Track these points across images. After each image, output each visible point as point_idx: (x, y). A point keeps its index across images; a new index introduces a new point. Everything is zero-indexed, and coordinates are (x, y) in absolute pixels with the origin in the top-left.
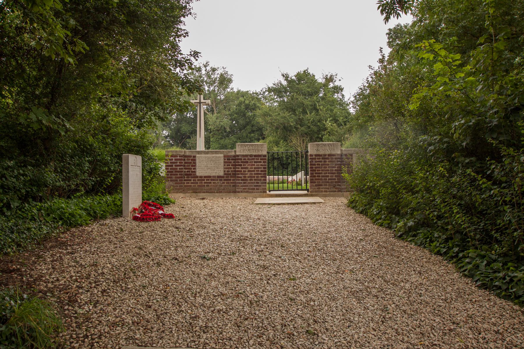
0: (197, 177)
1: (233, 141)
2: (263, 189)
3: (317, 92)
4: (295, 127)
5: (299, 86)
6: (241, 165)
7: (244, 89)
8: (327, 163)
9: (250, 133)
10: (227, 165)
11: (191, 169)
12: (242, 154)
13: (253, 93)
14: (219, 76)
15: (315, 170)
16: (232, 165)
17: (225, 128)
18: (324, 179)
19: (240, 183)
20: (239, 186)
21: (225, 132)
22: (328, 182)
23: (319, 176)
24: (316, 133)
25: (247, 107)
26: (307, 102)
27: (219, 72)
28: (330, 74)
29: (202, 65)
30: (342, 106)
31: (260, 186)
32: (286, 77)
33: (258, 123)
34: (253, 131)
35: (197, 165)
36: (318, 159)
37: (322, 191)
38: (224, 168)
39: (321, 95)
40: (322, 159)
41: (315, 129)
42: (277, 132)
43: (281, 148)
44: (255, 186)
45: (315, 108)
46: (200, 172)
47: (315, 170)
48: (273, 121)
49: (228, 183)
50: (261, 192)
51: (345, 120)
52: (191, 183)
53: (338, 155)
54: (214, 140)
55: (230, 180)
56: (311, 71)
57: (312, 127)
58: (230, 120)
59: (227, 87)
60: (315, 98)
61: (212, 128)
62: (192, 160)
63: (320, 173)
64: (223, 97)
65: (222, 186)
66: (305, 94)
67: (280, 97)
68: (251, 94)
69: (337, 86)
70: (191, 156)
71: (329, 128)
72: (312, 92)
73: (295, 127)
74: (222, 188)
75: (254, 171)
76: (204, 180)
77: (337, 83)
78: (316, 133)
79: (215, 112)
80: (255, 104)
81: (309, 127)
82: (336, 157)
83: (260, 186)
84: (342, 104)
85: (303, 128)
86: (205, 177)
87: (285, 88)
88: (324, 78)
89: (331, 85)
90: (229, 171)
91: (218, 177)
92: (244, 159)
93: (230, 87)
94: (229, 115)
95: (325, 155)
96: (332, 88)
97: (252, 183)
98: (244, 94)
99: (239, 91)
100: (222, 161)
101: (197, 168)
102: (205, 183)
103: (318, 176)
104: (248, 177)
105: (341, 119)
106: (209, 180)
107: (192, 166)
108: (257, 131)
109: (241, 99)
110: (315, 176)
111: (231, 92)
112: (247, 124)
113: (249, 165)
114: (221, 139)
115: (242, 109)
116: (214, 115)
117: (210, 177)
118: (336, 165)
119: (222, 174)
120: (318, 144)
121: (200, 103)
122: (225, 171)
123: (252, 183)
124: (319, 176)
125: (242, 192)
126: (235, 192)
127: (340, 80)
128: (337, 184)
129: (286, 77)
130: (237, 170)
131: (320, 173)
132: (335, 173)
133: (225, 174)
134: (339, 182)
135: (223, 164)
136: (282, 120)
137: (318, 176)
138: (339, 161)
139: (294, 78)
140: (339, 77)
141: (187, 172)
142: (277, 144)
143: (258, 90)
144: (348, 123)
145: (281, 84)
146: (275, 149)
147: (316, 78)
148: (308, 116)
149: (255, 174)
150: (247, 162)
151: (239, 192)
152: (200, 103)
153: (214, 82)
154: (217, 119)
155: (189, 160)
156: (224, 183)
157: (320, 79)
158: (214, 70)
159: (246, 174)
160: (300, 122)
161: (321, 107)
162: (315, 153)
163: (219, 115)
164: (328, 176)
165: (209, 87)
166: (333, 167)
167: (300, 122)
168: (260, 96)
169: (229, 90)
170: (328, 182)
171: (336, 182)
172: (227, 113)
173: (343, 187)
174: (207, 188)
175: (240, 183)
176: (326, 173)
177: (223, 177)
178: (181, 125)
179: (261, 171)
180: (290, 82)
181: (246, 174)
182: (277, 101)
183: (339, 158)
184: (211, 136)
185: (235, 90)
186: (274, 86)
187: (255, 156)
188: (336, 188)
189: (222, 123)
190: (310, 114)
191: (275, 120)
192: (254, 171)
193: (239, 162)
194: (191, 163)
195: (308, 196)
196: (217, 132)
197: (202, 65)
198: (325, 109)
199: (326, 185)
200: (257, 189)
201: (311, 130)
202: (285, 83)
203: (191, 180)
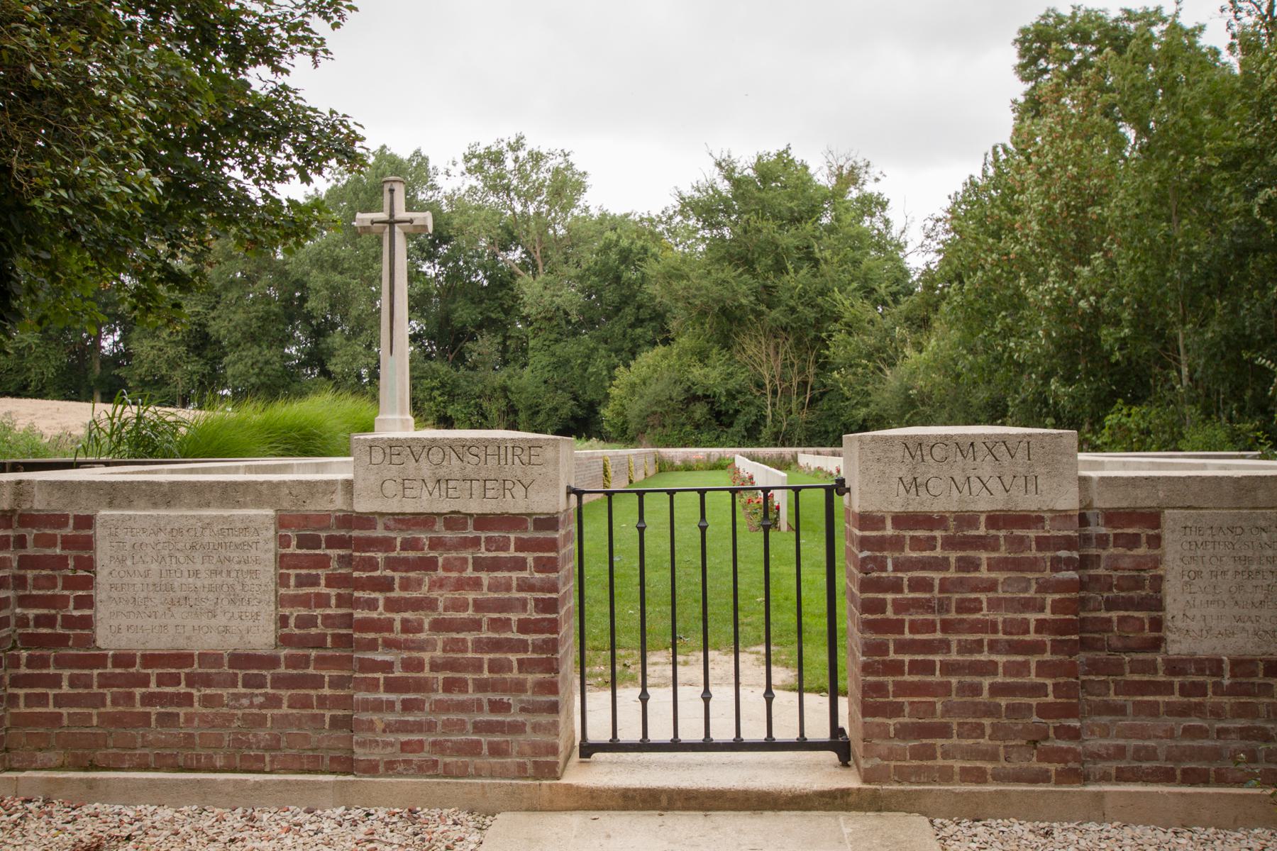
0: (99, 660)
1: (588, 348)
2: (537, 749)
3: (813, 211)
4: (753, 311)
5: (763, 195)
6: (385, 585)
7: (616, 210)
8: (984, 573)
9: (632, 326)
10: (301, 582)
11: (61, 602)
12: (394, 506)
13: (642, 220)
14: (549, 176)
15: (897, 626)
16: (330, 582)
17: (566, 313)
18: (962, 689)
19: (378, 706)
20: (370, 726)
21: (569, 322)
22: (992, 711)
23: (928, 668)
25: (625, 256)
26: (788, 239)
27: (553, 163)
28: (851, 162)
30: (885, 249)
31: (517, 728)
32: (726, 168)
33: (652, 298)
34: (639, 322)
35: (102, 576)
36: (917, 543)
37: (946, 775)
38: (281, 601)
39: (825, 221)
40: (949, 543)
41: (811, 314)
42: (702, 324)
43: (714, 368)
44: (479, 728)
45: (808, 256)
46: (121, 624)
47: (897, 626)
48: (693, 291)
49: (305, 703)
50: (521, 772)
51: (894, 288)
52: (60, 701)
53: (1063, 516)
55: (317, 682)
56: (797, 155)
57: (800, 308)
58: (582, 291)
59: (571, 204)
60: (809, 226)
61: (534, 311)
62: (67, 543)
63: (929, 647)
64: (561, 232)
65: (259, 721)
66: (780, 234)
67: (712, 226)
68: (635, 223)
69: (871, 195)
70: (60, 520)
71: (847, 314)
73: (753, 311)
75: (475, 625)
76: (144, 682)
77: (870, 188)
79: (540, 270)
80: (645, 250)
82: (1049, 531)
83: (517, 728)
84: (889, 248)
85: (774, 313)
86: (151, 660)
87: (725, 200)
88: (832, 174)
89: (854, 193)
90: (311, 621)
91: (241, 660)
92: (407, 545)
93: (580, 203)
94: (578, 277)
95: (967, 519)
96: (857, 200)
97: (462, 707)
98: (608, 222)
100: (266, 550)
101: (100, 594)
102: (149, 699)
103: (916, 667)
104: (435, 667)
106: (175, 680)
107: (70, 583)
108: (651, 319)
110: (896, 668)
111: (584, 218)
112: (625, 301)
113: (440, 584)
114: (557, 341)
115: (611, 262)
116: (539, 278)
117: (182, 659)
118: (1044, 587)
119: (260, 635)
120: (920, 442)
121: (392, 223)
122: (283, 621)
123: (462, 707)
124: (928, 668)
125: (390, 767)
126: (346, 765)
127: (877, 180)
129: (726, 168)
130: (359, 614)
131: (929, 647)
133: (285, 640)
134: (1071, 711)
135: (268, 572)
136: (716, 291)
137: (916, 667)
138: (1069, 564)
139: (750, 172)
140: (874, 171)
141: (39, 621)
142: (703, 357)
143: (656, 212)
144: (902, 298)
145: (716, 191)
146: (697, 372)
147: (811, 171)
148: (789, 279)
150: (430, 564)
151: (371, 769)
152: (392, 223)
153: (538, 192)
155: (51, 541)
156: (274, 702)
157: (823, 178)
158: (537, 158)
159: (421, 647)
160: (768, 295)
161: (827, 254)
162: (894, 501)
163: (551, 277)
164: (990, 668)
165: (525, 205)
166: (1027, 605)
167: (768, 295)
168: (660, 228)
169: (576, 212)
170: (992, 711)
171: (1044, 711)
172: (573, 272)
173: (1094, 743)
174: (163, 733)
175: (378, 706)
176: (977, 646)
177: (272, 662)
178: (453, 306)
179: (524, 626)
180: (737, 183)
181: (421, 647)
182: (704, 239)
183: (1069, 543)
185: (595, 212)
186: (697, 194)
187: (483, 521)
188: (1046, 756)
189: (558, 301)
190: (796, 272)
191: (698, 289)
192: (475, 625)
193: (372, 564)
194: (61, 562)
195: (847, 807)
196: (545, 324)
198: (836, 259)
199: (978, 730)
200: (496, 750)
202: (724, 187)
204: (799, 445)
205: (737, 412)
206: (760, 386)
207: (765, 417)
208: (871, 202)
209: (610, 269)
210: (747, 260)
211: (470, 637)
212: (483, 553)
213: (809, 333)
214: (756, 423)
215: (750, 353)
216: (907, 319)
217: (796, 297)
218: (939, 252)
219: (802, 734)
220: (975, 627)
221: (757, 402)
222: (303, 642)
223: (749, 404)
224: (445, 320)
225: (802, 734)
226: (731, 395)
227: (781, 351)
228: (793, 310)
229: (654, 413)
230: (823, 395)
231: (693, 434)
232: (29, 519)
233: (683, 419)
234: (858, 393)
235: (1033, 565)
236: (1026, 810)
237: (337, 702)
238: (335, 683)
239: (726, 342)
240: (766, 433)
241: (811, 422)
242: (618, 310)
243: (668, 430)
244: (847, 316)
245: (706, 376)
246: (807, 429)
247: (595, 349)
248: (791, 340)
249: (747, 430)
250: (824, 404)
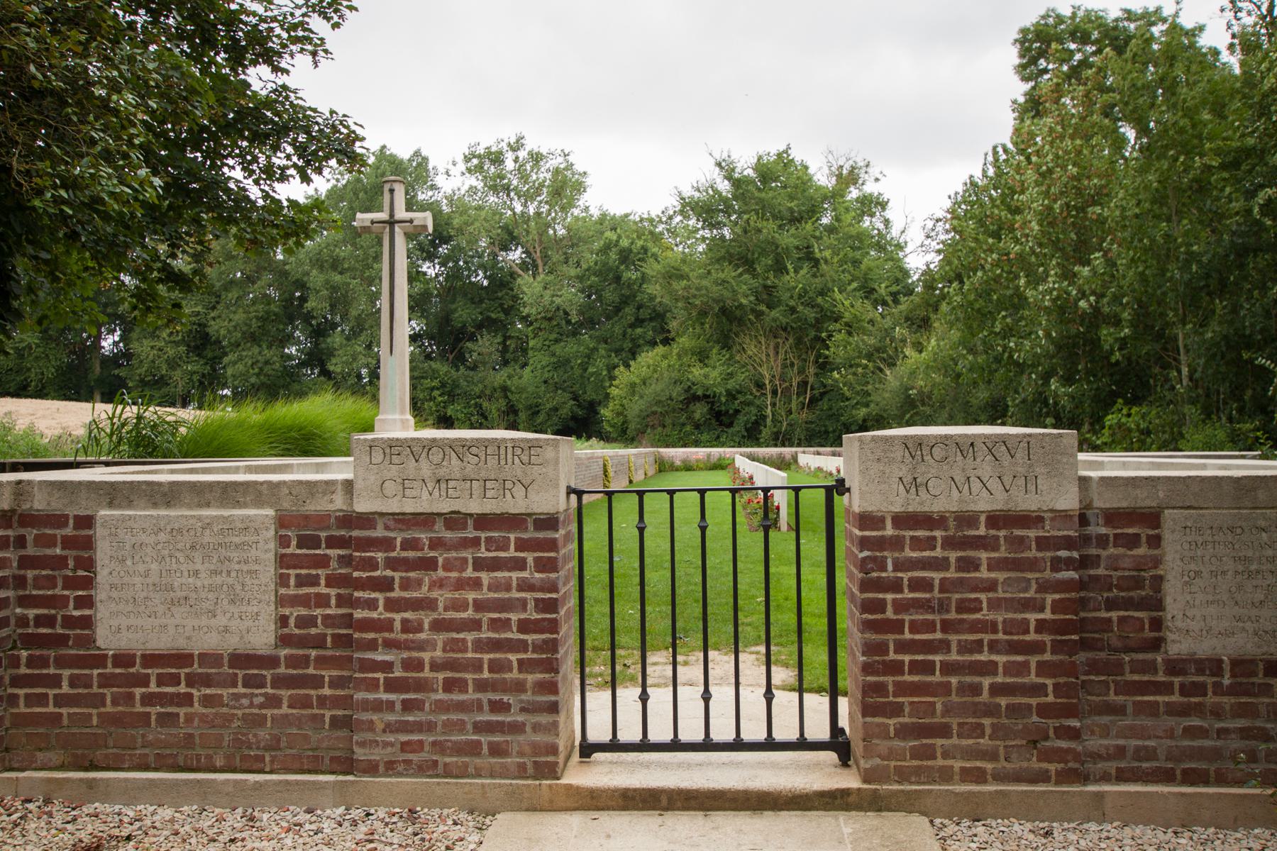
0: (100, 660)
2: (537, 749)
3: (813, 211)
4: (753, 311)
5: (763, 195)
6: (385, 585)
7: (617, 210)
8: (984, 573)
9: (632, 326)
10: (301, 581)
11: (61, 602)
12: (394, 506)
13: (642, 220)
14: (549, 176)
15: (897, 627)
17: (566, 313)
18: (962, 689)
19: (378, 706)
20: (370, 726)
21: (569, 322)
22: (991, 711)
23: (928, 668)
24: (812, 326)
26: (788, 239)
28: (851, 162)
29: (504, 145)
30: (885, 249)
31: (517, 728)
32: (726, 168)
33: (652, 298)
34: (639, 322)
35: (102, 576)
36: (917, 543)
37: (945, 775)
38: (281, 601)
39: (825, 221)
40: (949, 543)
41: (811, 314)
42: (702, 324)
43: (714, 368)
44: (479, 728)
45: (808, 256)
46: (121, 624)
47: (897, 627)
48: (693, 291)
49: (305, 703)
50: (521, 772)
51: (894, 288)
52: (60, 701)
53: (1062, 516)
54: (539, 345)
55: (317, 682)
56: (797, 155)
57: (800, 308)
58: (582, 291)
59: (571, 204)
60: (809, 226)
61: (534, 311)
62: (68, 543)
63: (929, 647)
64: (561, 232)
65: (260, 721)
66: (780, 233)
67: (712, 226)
68: (635, 223)
69: (871, 195)
70: (60, 520)
71: (847, 314)
72: (799, 212)
73: (753, 311)
74: (264, 734)
76: (144, 682)
77: (870, 188)
78: (812, 326)
79: (540, 270)
80: (645, 250)
81: (793, 310)
82: (1049, 531)
83: (517, 728)
84: (889, 248)
85: (774, 313)
86: (152, 659)
87: (725, 201)
88: (832, 174)
89: (854, 193)
90: (311, 621)
91: (241, 660)
92: (407, 545)
93: (580, 203)
94: (577, 277)
95: (967, 519)
96: (857, 200)
98: (616, 224)
99: (604, 216)
100: (265, 551)
101: (100, 595)
102: (148, 699)
103: (916, 667)
104: (435, 667)
105: (882, 290)
106: (175, 680)
107: (70, 583)
108: (651, 319)
109: (611, 235)
110: (896, 668)
111: (584, 218)
112: (625, 301)
113: (440, 584)
114: (557, 341)
115: (611, 261)
116: (539, 279)
117: (182, 659)
118: (1044, 587)
119: (260, 635)
120: (920, 442)
121: (392, 223)
122: (283, 621)
123: (461, 707)
124: (928, 668)
126: (347, 765)
127: (877, 180)
128: (1053, 723)
129: (726, 168)
130: (359, 614)
131: (929, 647)
132: (1037, 648)
133: (284, 640)
134: (1071, 711)
135: (268, 572)
137: (916, 667)
138: (1069, 564)
139: (750, 172)
140: (874, 171)
141: (39, 621)
142: (702, 356)
143: (655, 212)
144: (902, 299)
145: (716, 191)
146: (697, 372)
147: (811, 171)
148: (789, 279)
149: (480, 646)
150: (430, 564)
152: (392, 223)
153: (538, 191)
154: (545, 288)
155: (51, 542)
156: (274, 702)
157: (823, 178)
158: (537, 158)
159: (421, 646)
160: (768, 295)
161: (827, 254)
163: (551, 278)
164: (990, 668)
165: (525, 205)
166: (1027, 605)
167: (768, 295)
168: (660, 228)
169: (576, 212)
170: (991, 711)
171: (1043, 710)
172: (573, 272)
173: (1094, 743)
174: (163, 733)
175: (378, 706)
176: (977, 646)
177: (272, 661)
179: (524, 626)
180: (738, 183)
181: (421, 646)
182: (704, 239)
183: (1068, 543)
184: (531, 335)
185: (595, 213)
186: (697, 194)
187: (483, 521)
188: (1046, 756)
189: (558, 301)
190: (796, 272)
191: (698, 289)
192: (475, 625)
193: (372, 564)
194: (61, 562)
195: (847, 807)
196: (545, 324)
197: (504, 145)
198: (836, 260)
199: (978, 730)
200: (496, 750)
201: (799, 319)
202: (724, 187)
203: (55, 681)
204: (799, 445)
205: (737, 412)
206: (760, 386)
207: (765, 417)
208: (871, 202)
209: (610, 269)
210: (747, 260)
211: (470, 637)
212: (483, 553)
213: (809, 332)
214: (756, 423)
215: (750, 353)
216: (907, 319)
217: (796, 297)
218: (939, 252)
219: (802, 734)
220: (975, 627)
221: (757, 402)
222: (302, 642)
223: (749, 404)
224: (445, 319)
225: (802, 734)
226: (731, 395)
227: (782, 351)
228: (793, 310)
229: (654, 413)
230: (822, 394)
231: (693, 434)
233: (683, 419)
234: (858, 393)
236: (1027, 809)
237: (336, 702)
238: (334, 684)
239: (726, 342)
240: (766, 433)
241: (812, 422)
242: (618, 310)
243: (668, 430)
244: (847, 316)
245: (706, 376)
246: (807, 429)
247: (595, 349)
248: (791, 341)
249: (747, 430)
250: (824, 404)
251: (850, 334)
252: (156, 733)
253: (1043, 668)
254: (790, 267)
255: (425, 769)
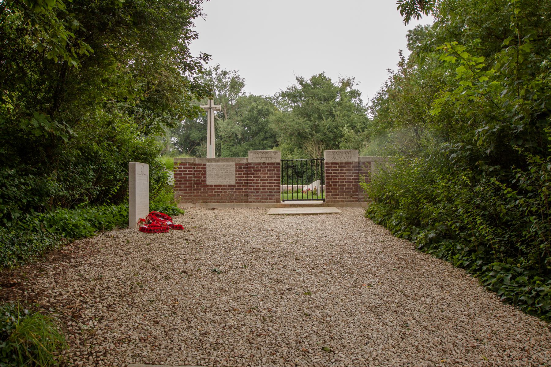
0: (207, 186)
2: (277, 199)
3: (333, 97)
4: (310, 134)
5: (314, 91)
6: (253, 174)
7: (256, 94)
8: (344, 171)
9: (263, 140)
10: (239, 174)
12: (254, 162)
13: (266, 98)
14: (230, 80)
15: (331, 179)
17: (236, 135)
18: (341, 188)
19: (252, 192)
20: (251, 195)
21: (237, 138)
22: (345, 192)
23: (336, 185)
25: (260, 113)
26: (323, 107)
27: (231, 75)
29: (212, 69)
30: (360, 111)
31: (273, 195)
32: (301, 81)
33: (271, 129)
34: (266, 138)
35: (207, 173)
36: (334, 167)
37: (338, 201)
38: (236, 177)
39: (338, 100)
40: (339, 167)
41: (331, 135)
42: (291, 139)
43: (296, 155)
44: (268, 196)
45: (331, 114)
46: (210, 181)
47: (331, 179)
48: (287, 127)
49: (240, 192)
51: (363, 126)
52: (201, 193)
53: (355, 162)
54: (225, 148)
55: (242, 189)
56: (327, 75)
57: (328, 133)
58: (242, 126)
59: (239, 91)
60: (331, 103)
61: (223, 134)
62: (202, 168)
63: (336, 182)
64: (234, 102)
65: (233, 195)
66: (320, 100)
67: (295, 102)
68: (264, 99)
69: (355, 90)
70: (200, 165)
71: (346, 135)
73: (310, 134)
74: (234, 197)
75: (267, 180)
76: (215, 189)
77: (355, 88)
79: (226, 118)
82: (354, 165)
83: (273, 195)
84: (360, 110)
85: (318, 135)
86: (216, 186)
87: (299, 93)
88: (340, 82)
89: (348, 89)
90: (241, 180)
91: (230, 186)
92: (257, 168)
93: (242, 91)
94: (241, 121)
95: (342, 163)
96: (350, 92)
97: (265, 192)
98: (257, 99)
99: (251, 96)
100: (234, 169)
101: (207, 176)
102: (215, 192)
103: (334, 185)
104: (261, 186)
106: (220, 189)
107: (202, 174)
108: (270, 137)
109: (254, 104)
110: (331, 186)
112: (260, 130)
113: (262, 174)
114: (233, 146)
115: (254, 115)
117: (221, 186)
118: (353, 173)
119: (233, 183)
121: (210, 108)
122: (236, 180)
123: (265, 192)
124: (336, 185)
125: (254, 202)
126: (247, 202)
127: (357, 84)
129: (301, 81)
130: (249, 178)
131: (336, 182)
133: (237, 183)
134: (357, 192)
135: (234, 172)
136: (296, 127)
137: (334, 185)
138: (357, 170)
139: (309, 82)
140: (356, 81)
141: (197, 180)
142: (291, 151)
143: (272, 95)
144: (365, 130)
145: (296, 89)
146: (290, 157)
147: (332, 82)
148: (324, 122)
149: (268, 183)
150: (260, 171)
151: (251, 202)
152: (210, 108)
153: (225, 86)
154: (228, 125)
155: (199, 168)
156: (235, 192)
157: (336, 83)
158: (225, 73)
160: (316, 128)
161: (338, 113)
163: (230, 121)
164: (345, 185)
165: (220, 91)
166: (350, 176)
167: (316, 128)
168: (273, 101)
169: (240, 94)
170: (345, 192)
171: (353, 191)
172: (239, 119)
173: (361, 197)
174: (218, 197)
175: (252, 192)
176: (343, 182)
177: (235, 186)
178: (191, 132)
179: (275, 180)
180: (305, 86)
182: (291, 107)
183: (357, 167)
184: (222, 143)
185: (248, 95)
186: (288, 91)
187: (268, 164)
188: (353, 198)
189: (233, 130)
190: (326, 119)
191: (289, 126)
192: (267, 180)
194: (200, 171)
195: (324, 206)
197: (212, 69)
198: (341, 115)
199: (343, 195)
200: (270, 199)
201: (327, 137)
202: (299, 87)
208: (355, 93)
210: (308, 115)
211: (266, 182)
212: (268, 169)
215: (309, 150)
220: (343, 179)
222: (239, 183)
224: (187, 137)
227: (321, 149)
232: (195, 164)
235: (351, 170)
236: (350, 206)
237: (245, 192)
238: (245, 189)
242: (257, 133)
244: (346, 136)
251: (346, 142)
252: (217, 197)
253: (353, 185)
254: (324, 118)
255: (260, 202)
